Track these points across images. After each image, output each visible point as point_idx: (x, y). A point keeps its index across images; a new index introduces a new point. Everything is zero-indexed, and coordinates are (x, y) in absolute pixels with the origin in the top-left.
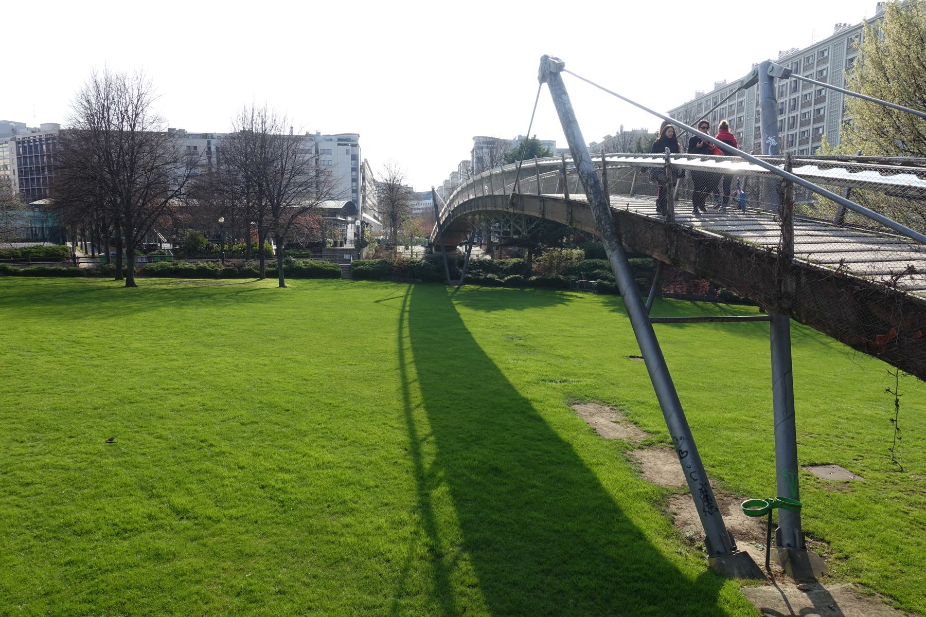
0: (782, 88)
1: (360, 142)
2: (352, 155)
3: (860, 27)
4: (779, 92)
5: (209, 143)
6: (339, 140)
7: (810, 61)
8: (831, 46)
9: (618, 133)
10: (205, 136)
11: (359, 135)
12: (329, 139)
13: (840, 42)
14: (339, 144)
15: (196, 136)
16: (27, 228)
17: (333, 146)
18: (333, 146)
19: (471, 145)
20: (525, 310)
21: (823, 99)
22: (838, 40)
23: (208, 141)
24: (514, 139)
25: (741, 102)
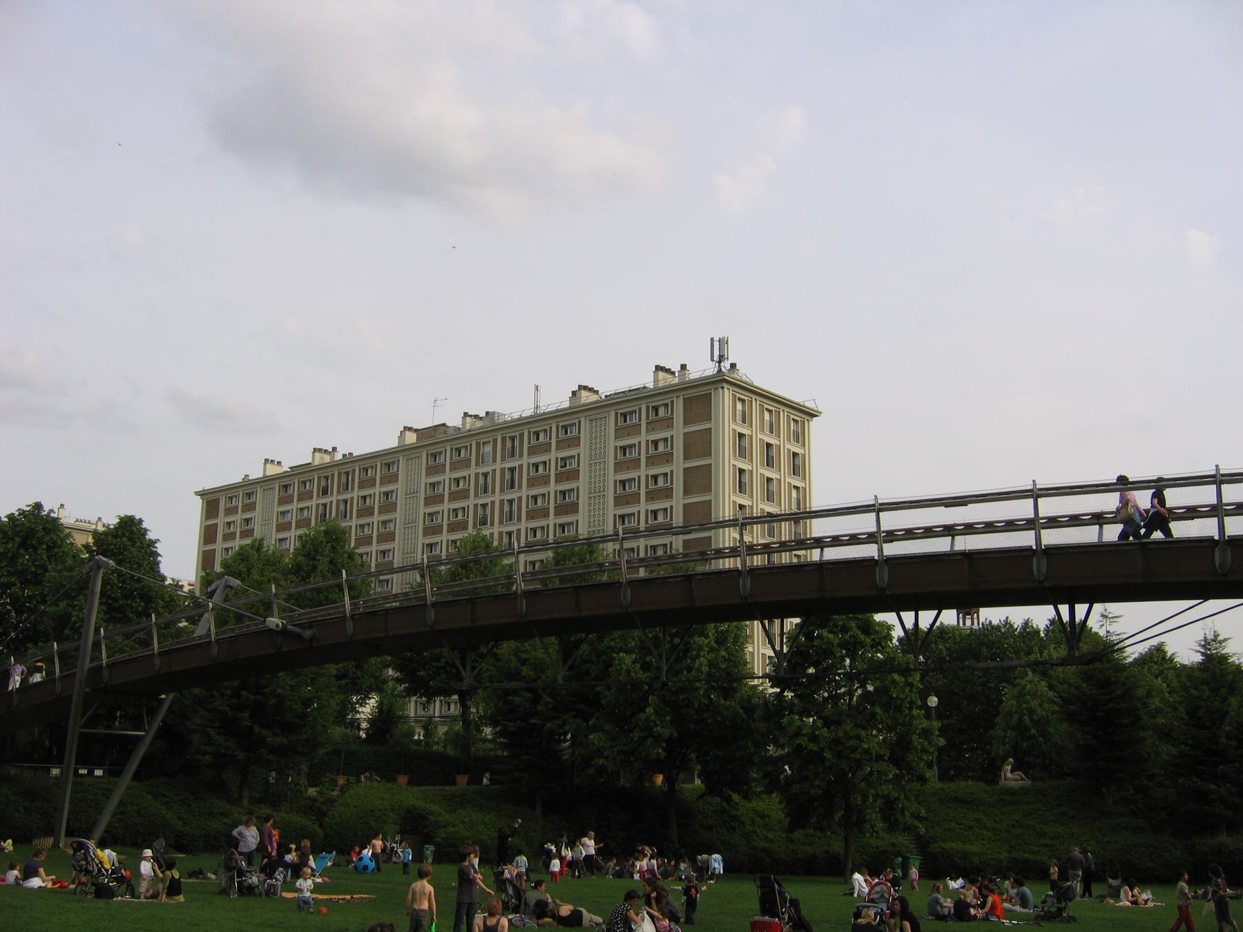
3: (386, 461)
13: (417, 455)
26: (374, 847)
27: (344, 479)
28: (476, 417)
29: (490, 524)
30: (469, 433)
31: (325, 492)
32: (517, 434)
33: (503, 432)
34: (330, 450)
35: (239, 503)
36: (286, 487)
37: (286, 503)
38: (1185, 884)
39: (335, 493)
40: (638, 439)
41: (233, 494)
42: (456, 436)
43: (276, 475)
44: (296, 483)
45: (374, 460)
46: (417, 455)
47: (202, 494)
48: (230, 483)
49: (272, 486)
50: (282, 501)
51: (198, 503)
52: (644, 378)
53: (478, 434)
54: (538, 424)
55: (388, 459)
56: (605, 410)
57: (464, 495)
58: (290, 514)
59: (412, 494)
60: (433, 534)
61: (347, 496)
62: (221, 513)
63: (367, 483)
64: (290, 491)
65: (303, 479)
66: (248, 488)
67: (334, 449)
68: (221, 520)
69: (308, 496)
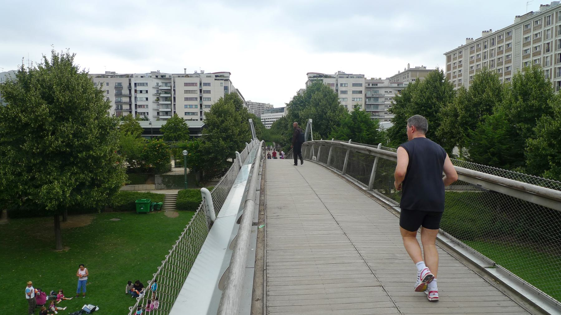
0: (485, 54)
1: (231, 78)
2: (224, 86)
3: (508, 31)
4: (483, 56)
5: (130, 80)
6: (216, 76)
7: (501, 38)
8: (513, 29)
9: (405, 69)
10: (127, 76)
11: (230, 74)
12: (209, 76)
13: (519, 27)
14: (215, 79)
15: (122, 76)
16: (103, 182)
17: (211, 80)
18: (211, 80)
19: (306, 79)
20: (184, 211)
21: (510, 61)
22: (516, 27)
23: (129, 79)
24: (335, 74)
25: (460, 62)
26: (549, 159)
27: (492, 41)
28: (547, 5)
29: (551, 51)
30: (541, 14)
31: (485, 47)
32: (551, 14)
33: (545, 15)
34: (489, 31)
35: (457, 55)
36: (527, 26)
37: (472, 53)
38: (238, 152)
39: (489, 47)
40: (541, 30)
41: (509, 31)
42: (557, 7)
43: (508, 27)
44: (475, 46)
45: (502, 32)
46: (519, 27)
47: (446, 54)
48: (507, 26)
49: (467, 48)
50: (471, 53)
51: (445, 57)
52: (480, 35)
53: (545, 13)
54: (499, 34)
55: (499, 34)
56: (538, 17)
57: (539, 40)
58: (474, 57)
59: (517, 43)
60: (527, 58)
61: (493, 48)
62: (452, 60)
63: (500, 41)
64: (529, 27)
65: (478, 44)
66: (460, 50)
67: (491, 30)
68: (452, 62)
69: (502, 41)
